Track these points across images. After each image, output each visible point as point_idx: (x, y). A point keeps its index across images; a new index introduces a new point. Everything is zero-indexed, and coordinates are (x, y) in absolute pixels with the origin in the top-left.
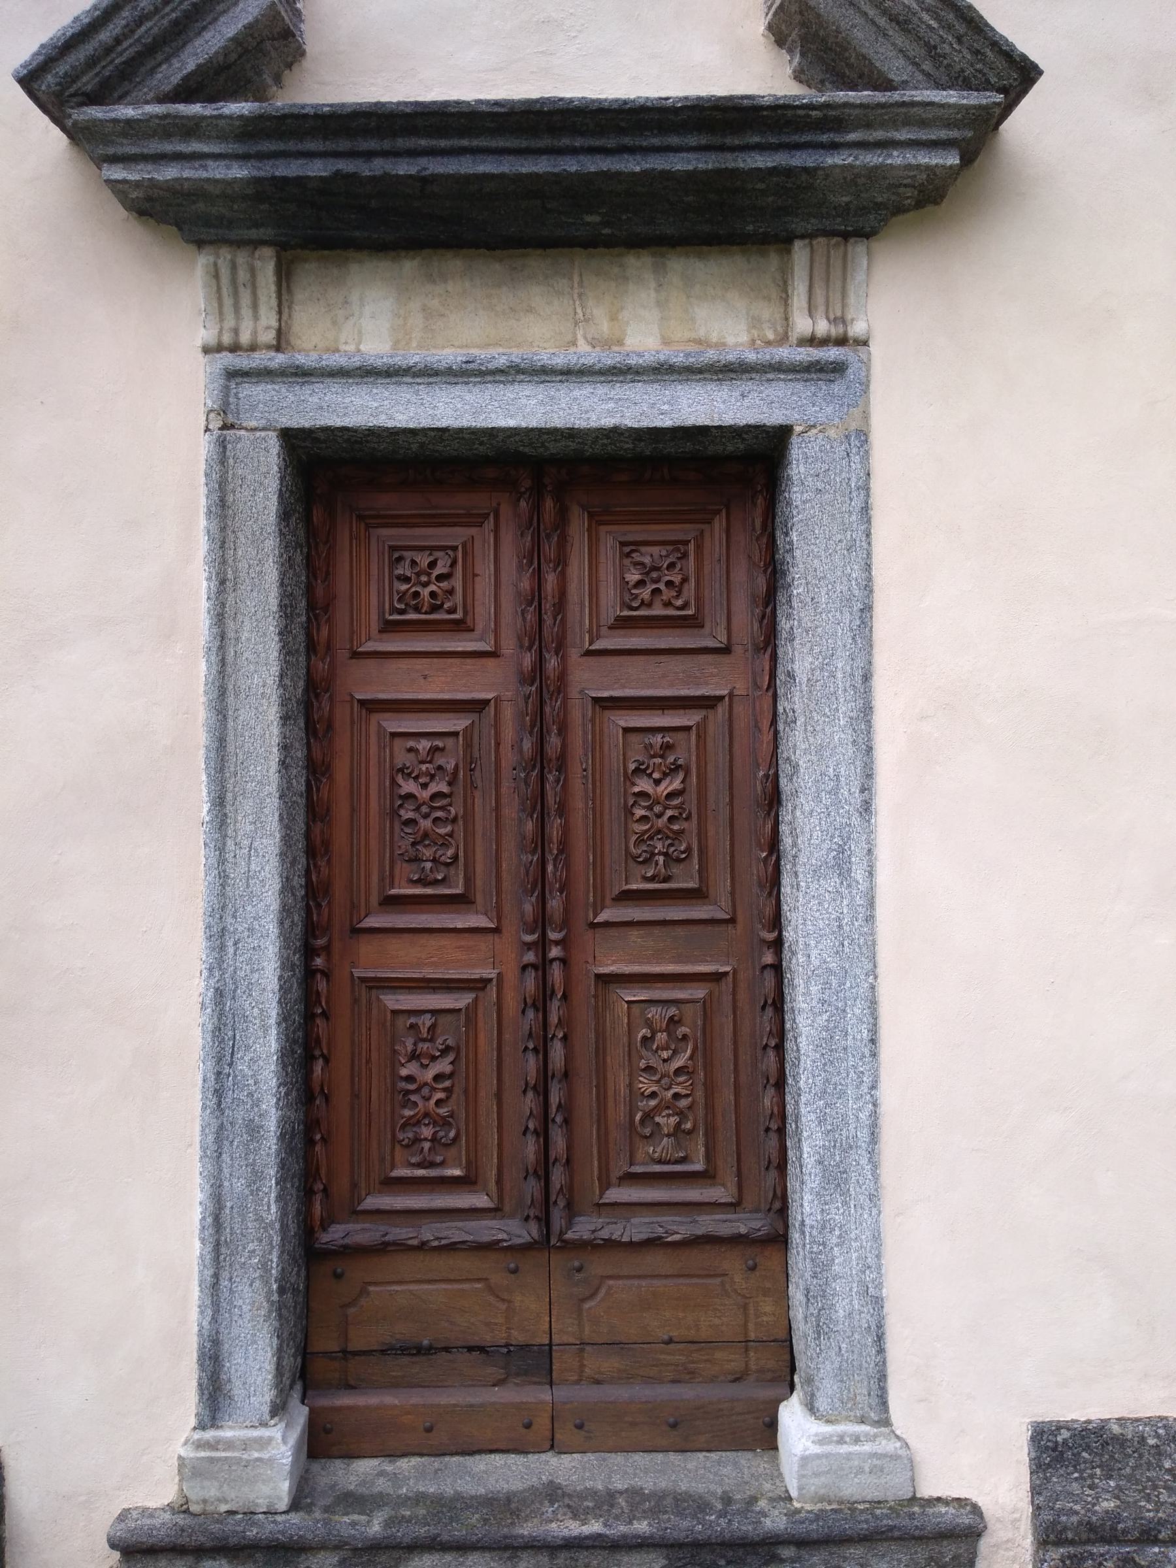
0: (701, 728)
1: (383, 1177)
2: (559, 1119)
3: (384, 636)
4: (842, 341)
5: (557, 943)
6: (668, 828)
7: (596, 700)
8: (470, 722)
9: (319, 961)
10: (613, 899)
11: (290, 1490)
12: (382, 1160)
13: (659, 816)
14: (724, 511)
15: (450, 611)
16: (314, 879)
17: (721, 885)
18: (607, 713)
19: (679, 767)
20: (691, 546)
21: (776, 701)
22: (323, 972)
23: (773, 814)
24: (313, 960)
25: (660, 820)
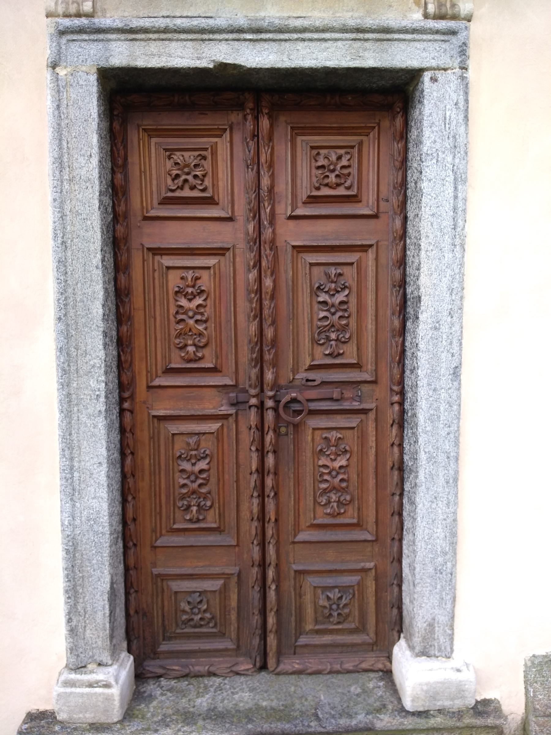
0: (359, 262)
1: (164, 368)
2: (272, 494)
3: (161, 206)
4: (455, 17)
5: (270, 398)
6: (340, 486)
7: (294, 247)
8: (220, 424)
9: (126, 405)
10: (304, 203)
11: (121, 694)
12: (168, 518)
13: (333, 314)
14: (376, 128)
15: (203, 190)
16: (121, 311)
17: (369, 196)
18: (301, 255)
19: (346, 451)
20: (356, 149)
21: (403, 484)
22: (128, 410)
23: (403, 192)
24: (123, 404)
25: (334, 317)
